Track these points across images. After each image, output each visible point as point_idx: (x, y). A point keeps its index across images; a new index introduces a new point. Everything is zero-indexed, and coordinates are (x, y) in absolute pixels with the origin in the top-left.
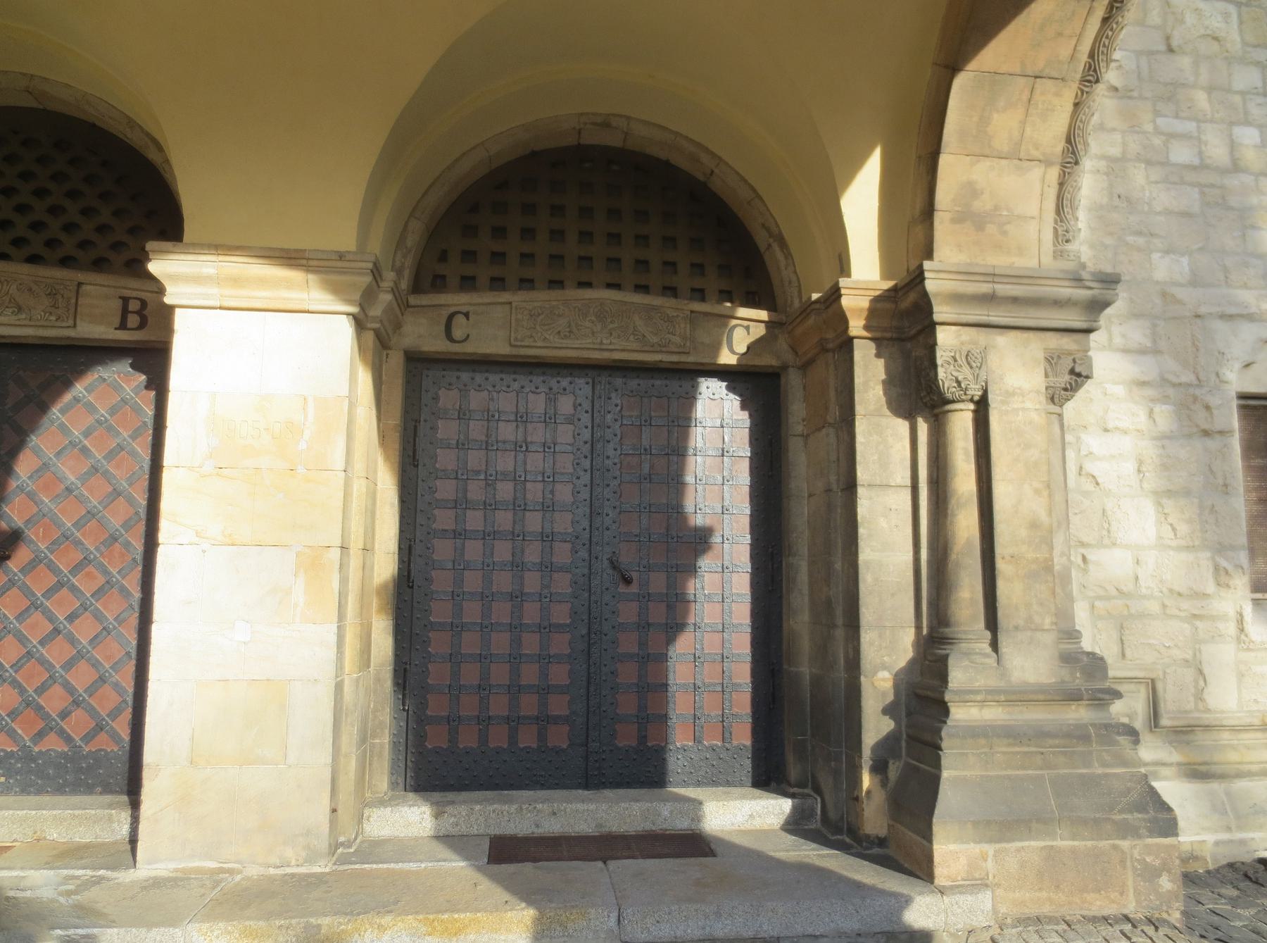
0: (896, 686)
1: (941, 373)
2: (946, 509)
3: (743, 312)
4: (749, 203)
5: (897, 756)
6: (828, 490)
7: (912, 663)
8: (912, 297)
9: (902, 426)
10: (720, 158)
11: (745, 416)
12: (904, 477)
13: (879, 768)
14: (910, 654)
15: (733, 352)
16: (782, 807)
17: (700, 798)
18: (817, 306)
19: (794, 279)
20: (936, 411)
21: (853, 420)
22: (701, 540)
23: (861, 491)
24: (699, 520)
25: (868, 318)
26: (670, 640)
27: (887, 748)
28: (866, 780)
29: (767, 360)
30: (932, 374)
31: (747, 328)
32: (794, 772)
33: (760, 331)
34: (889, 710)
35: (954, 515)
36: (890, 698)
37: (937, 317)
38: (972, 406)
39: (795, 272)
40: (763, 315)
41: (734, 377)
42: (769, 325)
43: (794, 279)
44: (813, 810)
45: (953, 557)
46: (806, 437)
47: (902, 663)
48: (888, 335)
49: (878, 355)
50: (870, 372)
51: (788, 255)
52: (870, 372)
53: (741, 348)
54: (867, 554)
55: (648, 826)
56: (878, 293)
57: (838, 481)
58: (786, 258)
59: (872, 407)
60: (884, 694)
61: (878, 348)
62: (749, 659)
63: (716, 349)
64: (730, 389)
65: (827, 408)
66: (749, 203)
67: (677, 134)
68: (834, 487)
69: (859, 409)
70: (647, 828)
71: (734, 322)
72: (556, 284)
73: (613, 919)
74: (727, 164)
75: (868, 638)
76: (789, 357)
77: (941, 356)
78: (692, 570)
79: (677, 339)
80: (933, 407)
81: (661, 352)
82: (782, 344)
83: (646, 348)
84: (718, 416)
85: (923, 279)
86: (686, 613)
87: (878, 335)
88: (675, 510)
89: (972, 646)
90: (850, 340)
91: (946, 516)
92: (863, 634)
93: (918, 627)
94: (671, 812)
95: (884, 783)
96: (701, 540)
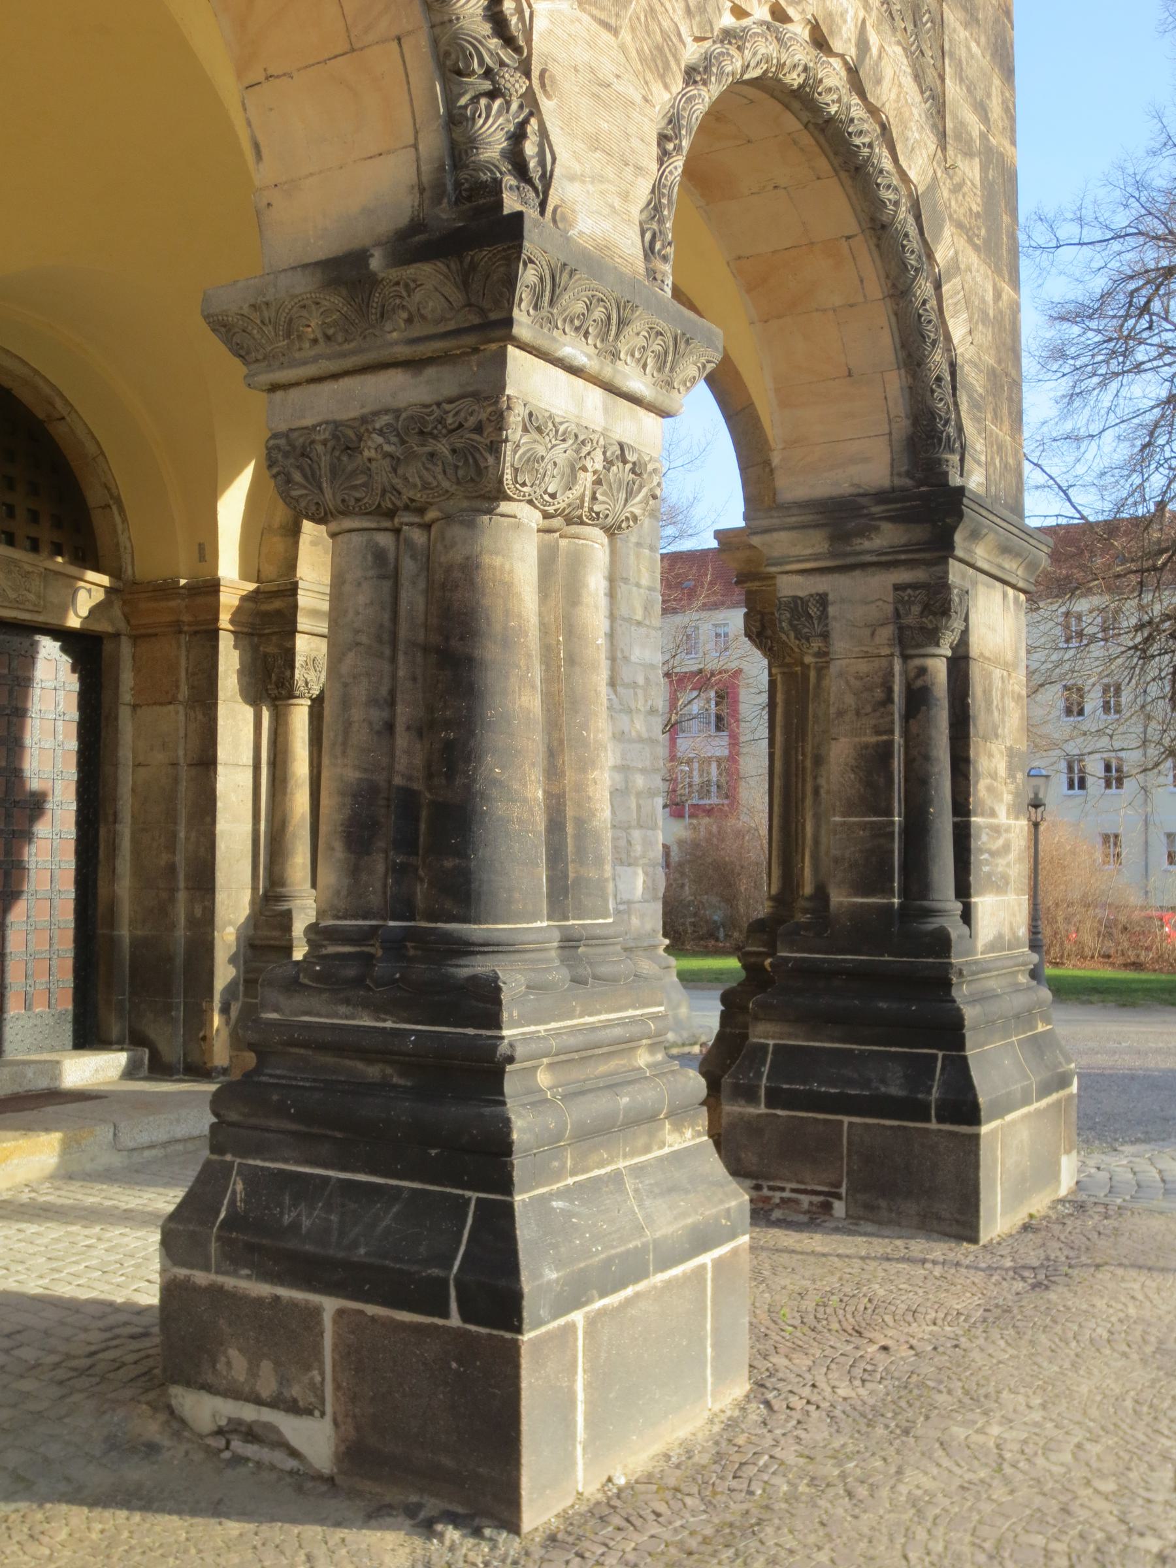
0: (238, 939)
1: (298, 674)
2: (286, 788)
3: (91, 575)
4: (94, 459)
5: (237, 999)
6: (174, 765)
7: (248, 918)
8: (277, 604)
9: (248, 712)
10: (71, 405)
11: (75, 677)
12: (247, 757)
13: (225, 1010)
14: (247, 912)
15: (78, 616)
16: (120, 1059)
17: (58, 1058)
18: (182, 591)
19: (128, 545)
20: (277, 703)
21: (216, 704)
22: (36, 805)
23: (220, 769)
24: (34, 784)
25: (234, 614)
26: (6, 910)
27: (231, 989)
28: (217, 1020)
29: (103, 626)
30: (288, 673)
31: (89, 591)
32: (115, 1030)
33: (99, 595)
34: (233, 960)
35: (292, 794)
36: (234, 949)
37: (300, 627)
38: (309, 703)
39: (129, 538)
40: (105, 580)
41: (71, 641)
42: (109, 591)
43: (128, 545)
44: (142, 1060)
45: (291, 828)
46: (135, 707)
47: (242, 919)
48: (245, 630)
49: (236, 647)
50: (229, 660)
51: (125, 520)
52: (229, 660)
53: (84, 611)
54: (222, 826)
55: (16, 1089)
56: (245, 593)
57: (185, 755)
58: (123, 522)
59: (229, 694)
60: (230, 947)
61: (236, 640)
62: (73, 925)
63: (63, 610)
64: (64, 649)
65: (177, 687)
66: (94, 459)
67: (36, 371)
68: (182, 761)
69: (221, 694)
70: (15, 1091)
71: (81, 584)
72: (34, 546)
73: (111, 1134)
74: (76, 412)
75: (221, 897)
76: (122, 625)
77: (299, 660)
78: (27, 836)
79: (32, 597)
80: (276, 699)
81: (18, 609)
82: (117, 611)
83: (6, 604)
84: (53, 676)
85: (295, 594)
86: (21, 880)
87: (239, 629)
88: (15, 774)
89: (304, 902)
90: (217, 630)
91: (285, 793)
92: (217, 895)
93: (255, 888)
94: (35, 1073)
95: (227, 1023)
96: (36, 805)
